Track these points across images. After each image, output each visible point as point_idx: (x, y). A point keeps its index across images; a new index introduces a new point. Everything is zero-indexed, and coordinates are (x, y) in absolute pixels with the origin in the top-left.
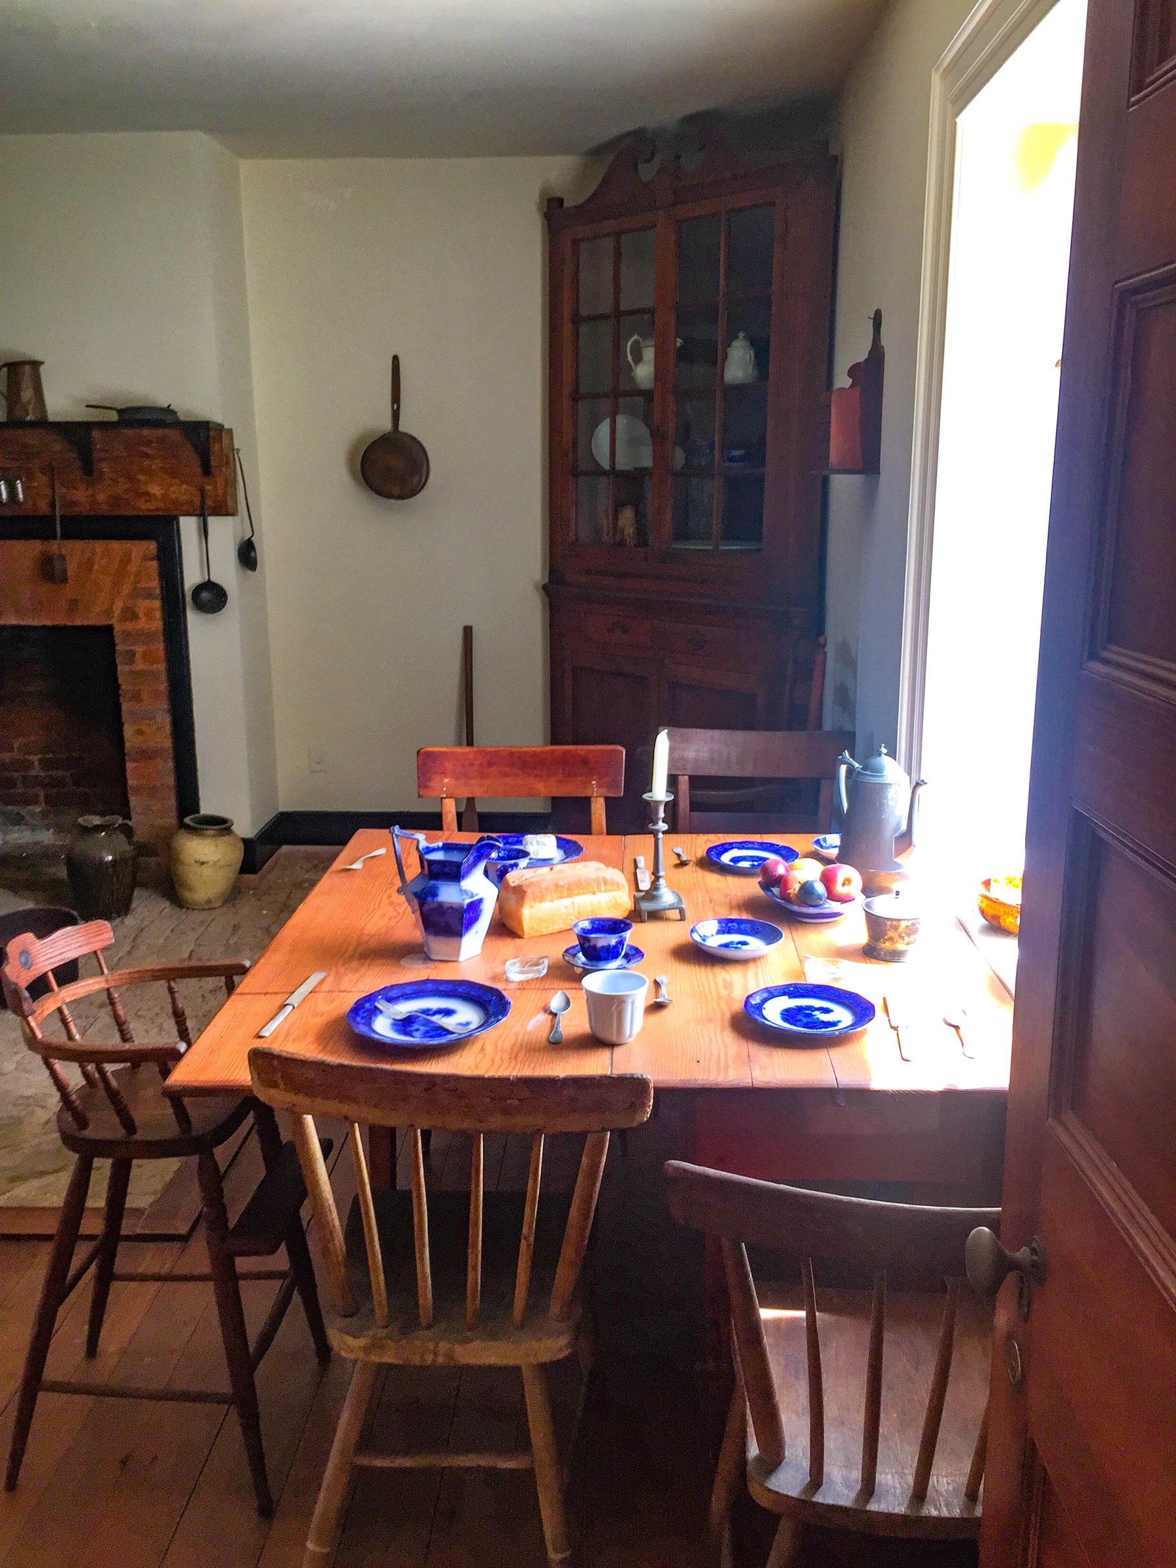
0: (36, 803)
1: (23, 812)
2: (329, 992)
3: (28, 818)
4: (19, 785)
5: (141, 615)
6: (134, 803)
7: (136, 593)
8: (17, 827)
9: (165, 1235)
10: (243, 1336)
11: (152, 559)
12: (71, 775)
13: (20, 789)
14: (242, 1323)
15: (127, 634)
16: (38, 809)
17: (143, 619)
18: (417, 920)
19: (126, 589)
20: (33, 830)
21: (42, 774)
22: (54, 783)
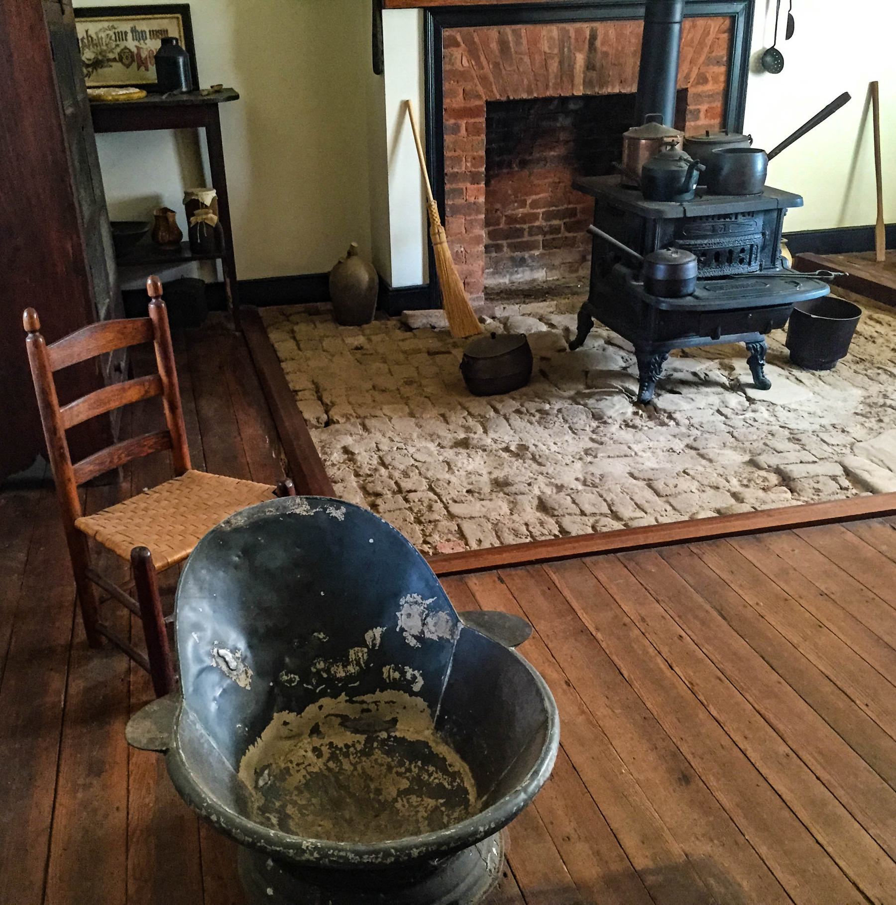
0: (537, 248)
1: (526, 255)
2: (722, 745)
3: (530, 261)
4: (526, 233)
5: (710, 79)
6: (69, 589)
7: (709, 61)
8: (521, 269)
9: (632, 547)
10: (713, 518)
11: (725, 32)
12: (564, 223)
13: (526, 238)
14: (709, 518)
15: (698, 96)
16: (537, 253)
17: (711, 83)
18: (864, 259)
19: (703, 58)
20: (532, 270)
21: (544, 224)
22: (555, 230)
